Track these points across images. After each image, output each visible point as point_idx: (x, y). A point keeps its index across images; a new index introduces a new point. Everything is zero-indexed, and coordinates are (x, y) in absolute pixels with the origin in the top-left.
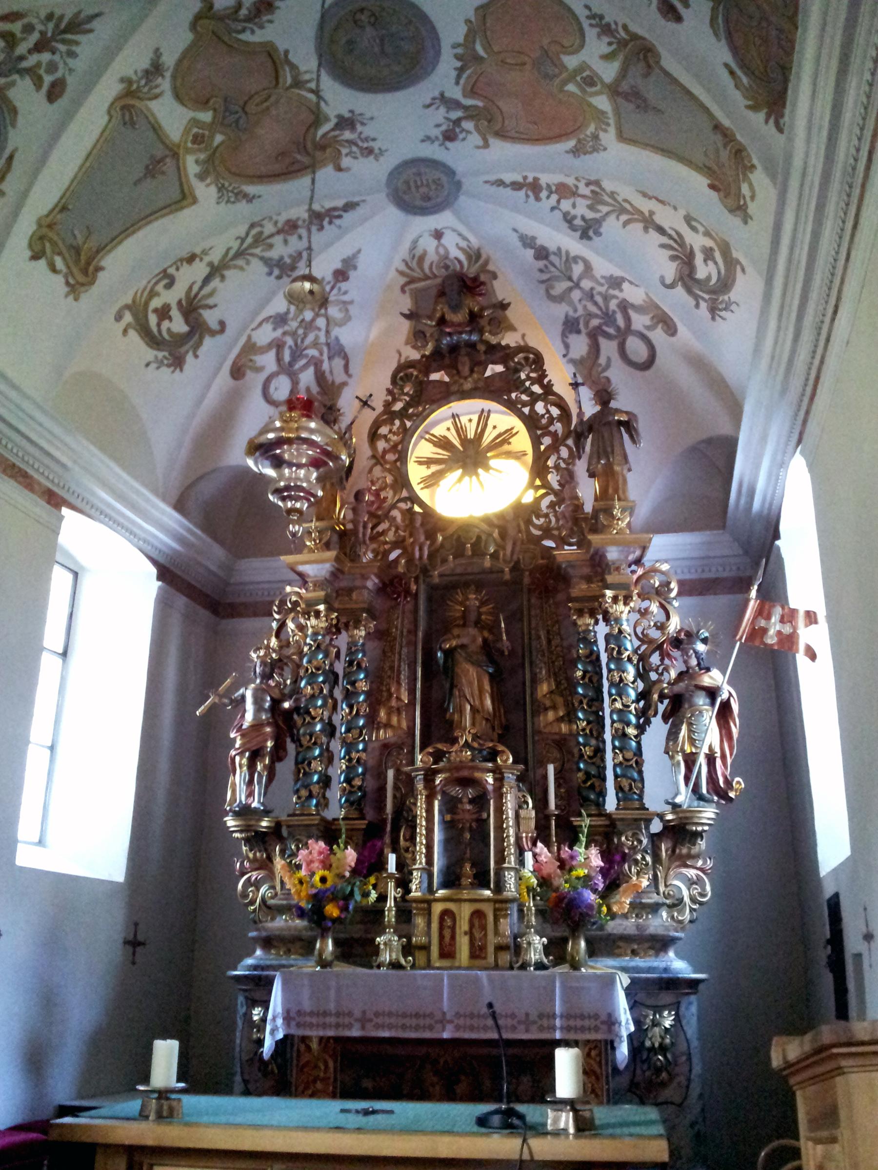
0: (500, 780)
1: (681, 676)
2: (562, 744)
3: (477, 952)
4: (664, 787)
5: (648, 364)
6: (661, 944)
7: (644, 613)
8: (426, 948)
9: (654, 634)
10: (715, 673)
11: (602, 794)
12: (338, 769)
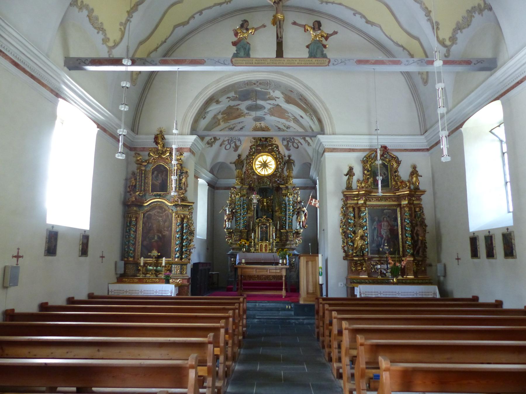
0: (270, 225)
1: (300, 208)
2: (280, 218)
3: (266, 250)
4: (296, 226)
5: (298, 148)
6: (293, 249)
7: (294, 197)
8: (258, 250)
9: (295, 200)
10: (305, 208)
11: (286, 226)
12: (242, 221)
